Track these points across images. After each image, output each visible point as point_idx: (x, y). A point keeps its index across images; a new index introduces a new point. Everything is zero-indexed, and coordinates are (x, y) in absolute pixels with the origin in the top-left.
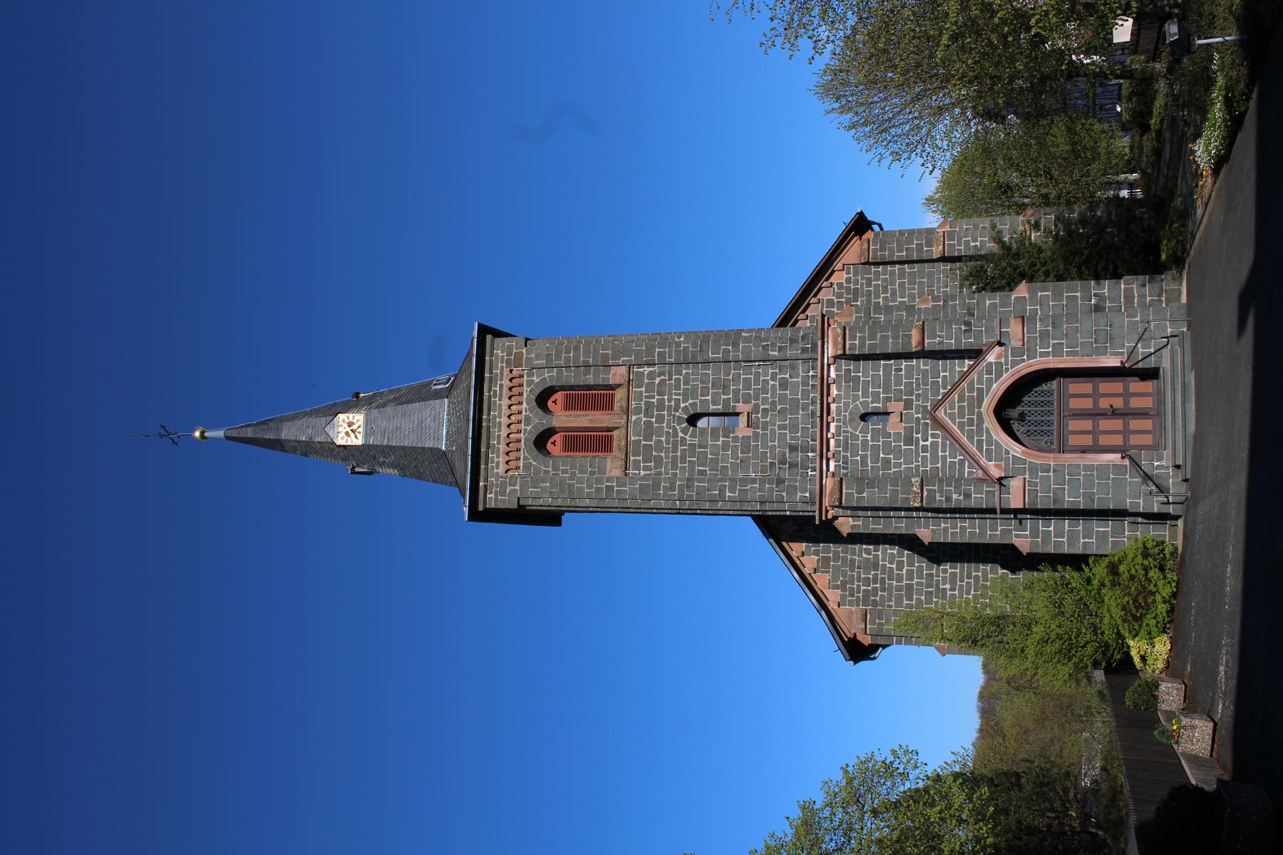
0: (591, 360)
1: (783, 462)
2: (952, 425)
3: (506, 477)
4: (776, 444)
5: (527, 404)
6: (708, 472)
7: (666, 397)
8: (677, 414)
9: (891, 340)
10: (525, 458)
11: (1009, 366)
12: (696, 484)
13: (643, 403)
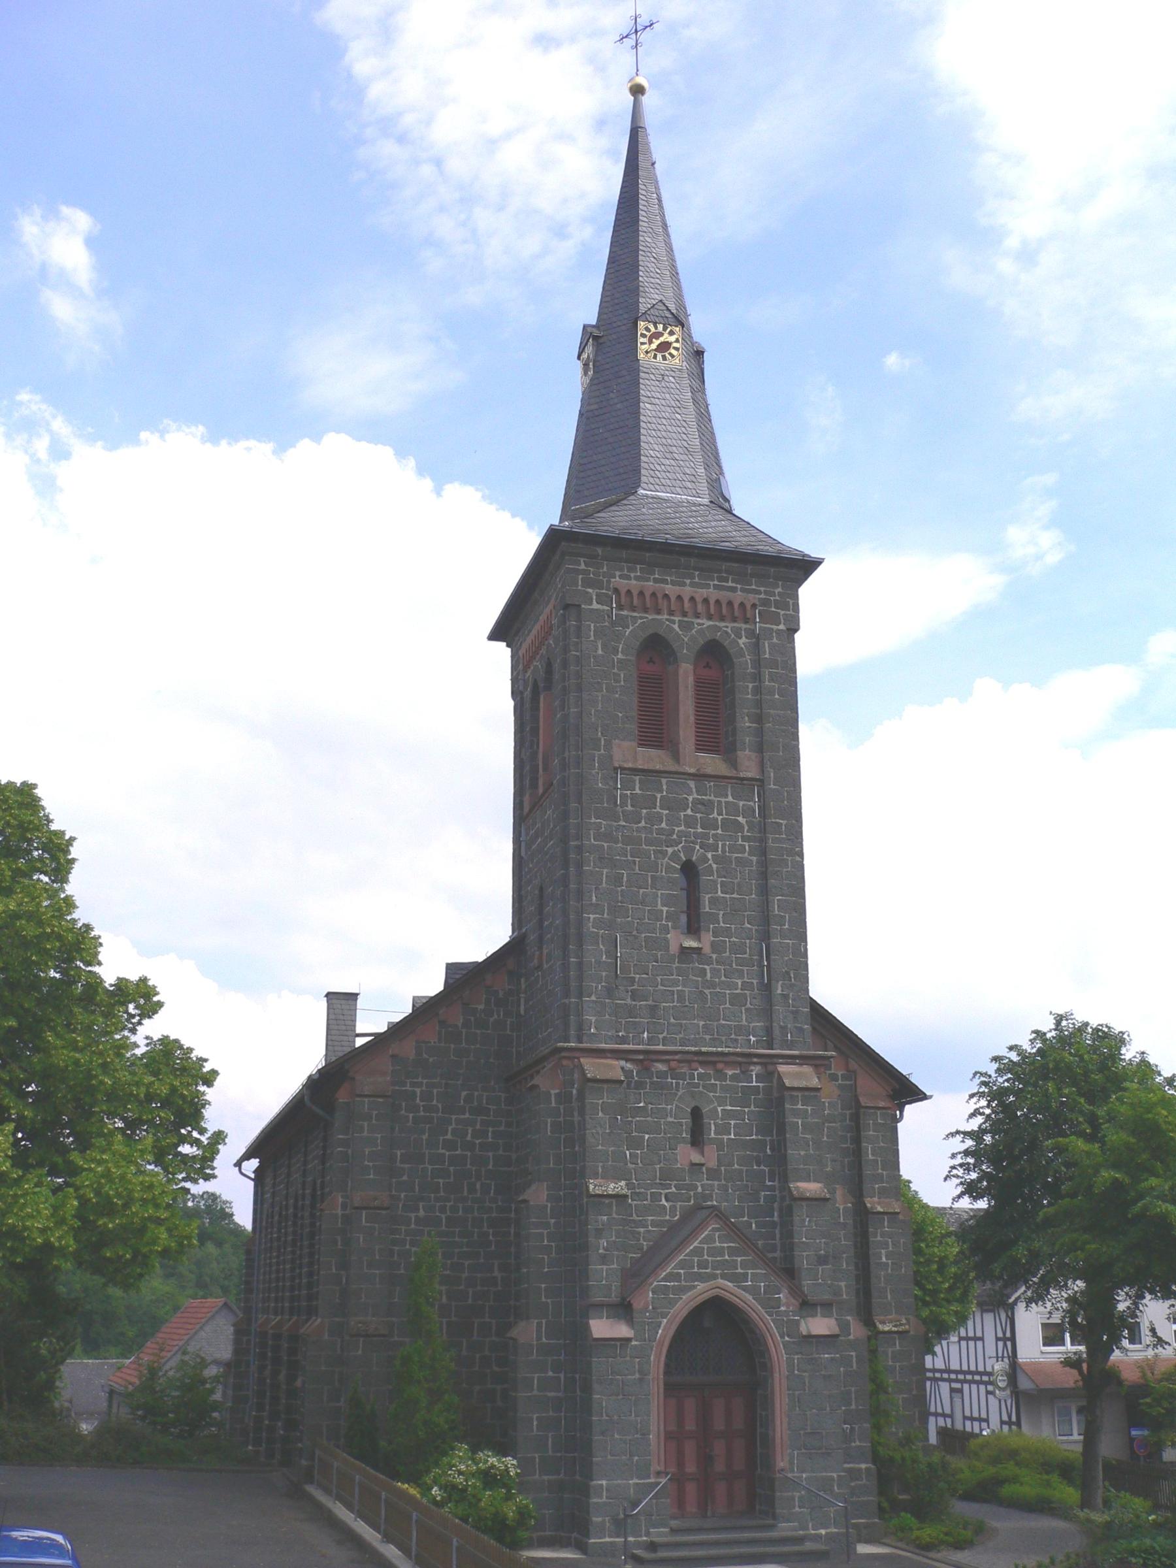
2: (700, 1239)
6: (619, 889)
7: (719, 831)
9: (802, 1153)
12: (605, 871)
13: (712, 798)
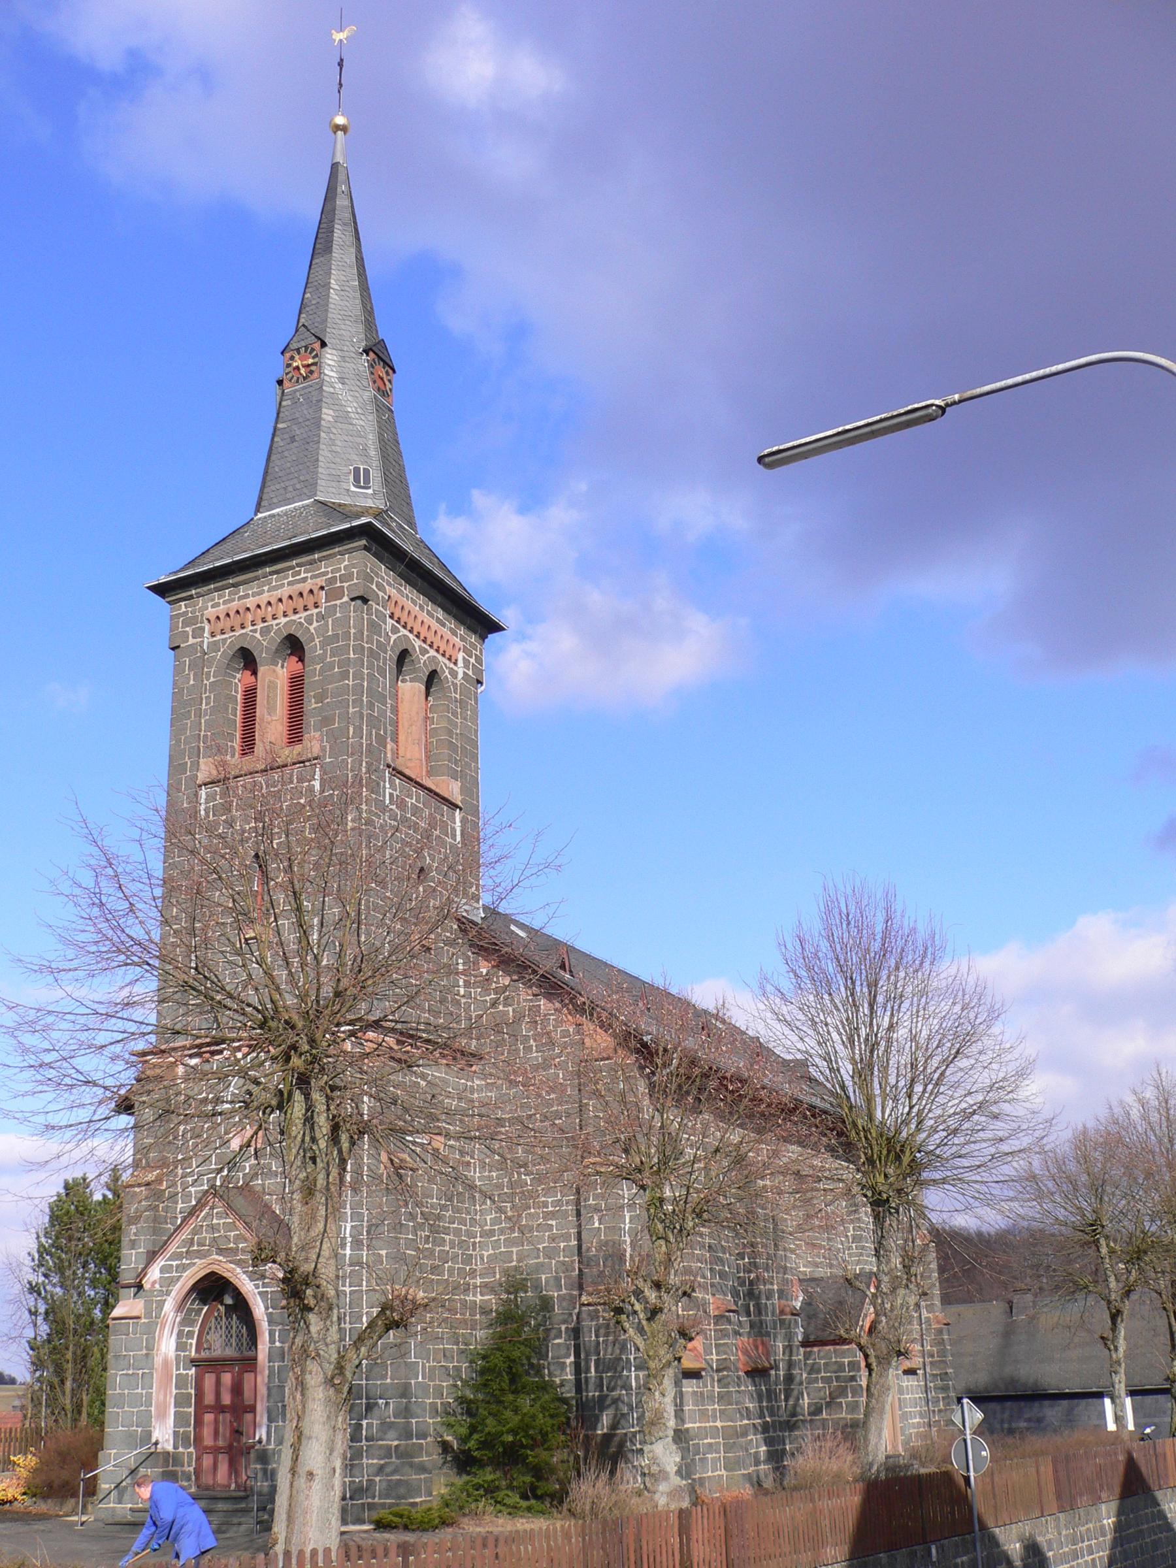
0: (328, 700)
10: (225, 640)
11: (261, 1289)
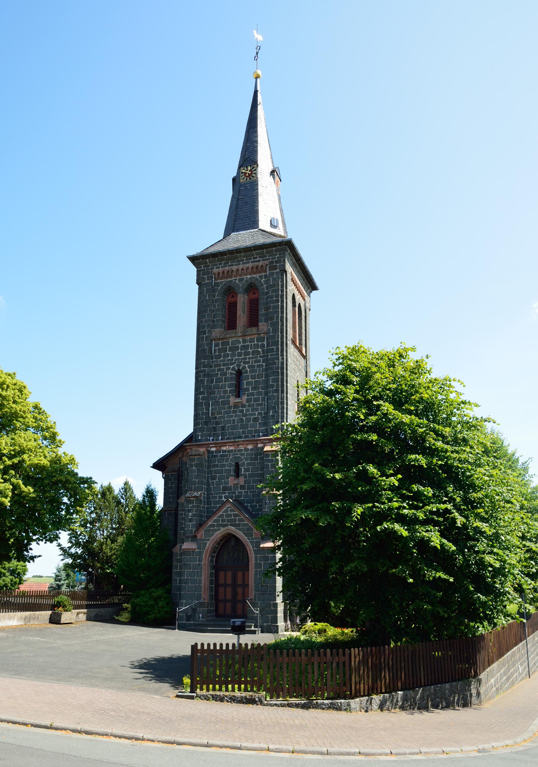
1: (217, 423)
3: (212, 274)
4: (226, 419)
5: (250, 278)
8: (242, 364)
12: (206, 379)
13: (248, 343)
